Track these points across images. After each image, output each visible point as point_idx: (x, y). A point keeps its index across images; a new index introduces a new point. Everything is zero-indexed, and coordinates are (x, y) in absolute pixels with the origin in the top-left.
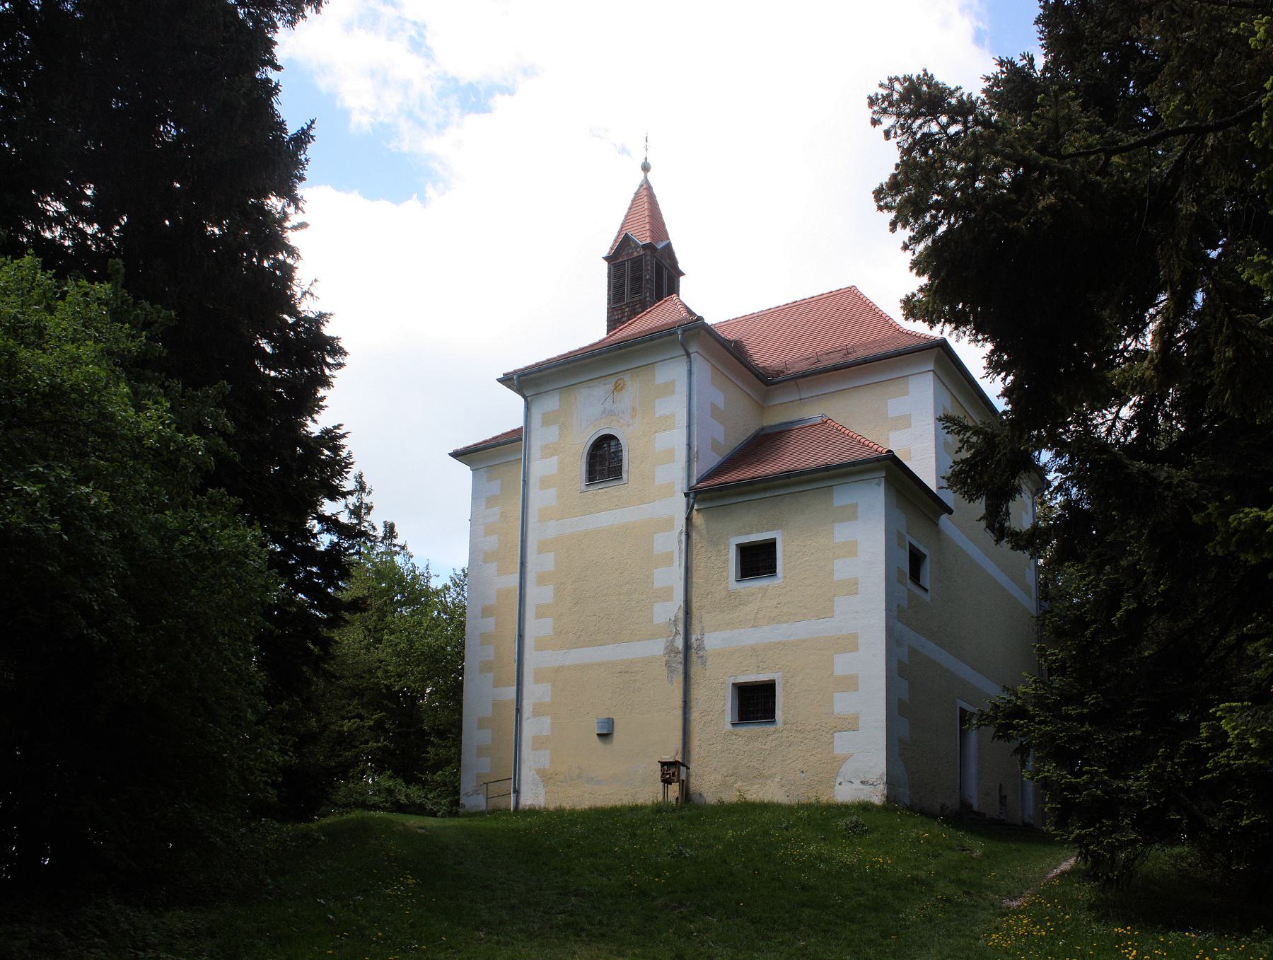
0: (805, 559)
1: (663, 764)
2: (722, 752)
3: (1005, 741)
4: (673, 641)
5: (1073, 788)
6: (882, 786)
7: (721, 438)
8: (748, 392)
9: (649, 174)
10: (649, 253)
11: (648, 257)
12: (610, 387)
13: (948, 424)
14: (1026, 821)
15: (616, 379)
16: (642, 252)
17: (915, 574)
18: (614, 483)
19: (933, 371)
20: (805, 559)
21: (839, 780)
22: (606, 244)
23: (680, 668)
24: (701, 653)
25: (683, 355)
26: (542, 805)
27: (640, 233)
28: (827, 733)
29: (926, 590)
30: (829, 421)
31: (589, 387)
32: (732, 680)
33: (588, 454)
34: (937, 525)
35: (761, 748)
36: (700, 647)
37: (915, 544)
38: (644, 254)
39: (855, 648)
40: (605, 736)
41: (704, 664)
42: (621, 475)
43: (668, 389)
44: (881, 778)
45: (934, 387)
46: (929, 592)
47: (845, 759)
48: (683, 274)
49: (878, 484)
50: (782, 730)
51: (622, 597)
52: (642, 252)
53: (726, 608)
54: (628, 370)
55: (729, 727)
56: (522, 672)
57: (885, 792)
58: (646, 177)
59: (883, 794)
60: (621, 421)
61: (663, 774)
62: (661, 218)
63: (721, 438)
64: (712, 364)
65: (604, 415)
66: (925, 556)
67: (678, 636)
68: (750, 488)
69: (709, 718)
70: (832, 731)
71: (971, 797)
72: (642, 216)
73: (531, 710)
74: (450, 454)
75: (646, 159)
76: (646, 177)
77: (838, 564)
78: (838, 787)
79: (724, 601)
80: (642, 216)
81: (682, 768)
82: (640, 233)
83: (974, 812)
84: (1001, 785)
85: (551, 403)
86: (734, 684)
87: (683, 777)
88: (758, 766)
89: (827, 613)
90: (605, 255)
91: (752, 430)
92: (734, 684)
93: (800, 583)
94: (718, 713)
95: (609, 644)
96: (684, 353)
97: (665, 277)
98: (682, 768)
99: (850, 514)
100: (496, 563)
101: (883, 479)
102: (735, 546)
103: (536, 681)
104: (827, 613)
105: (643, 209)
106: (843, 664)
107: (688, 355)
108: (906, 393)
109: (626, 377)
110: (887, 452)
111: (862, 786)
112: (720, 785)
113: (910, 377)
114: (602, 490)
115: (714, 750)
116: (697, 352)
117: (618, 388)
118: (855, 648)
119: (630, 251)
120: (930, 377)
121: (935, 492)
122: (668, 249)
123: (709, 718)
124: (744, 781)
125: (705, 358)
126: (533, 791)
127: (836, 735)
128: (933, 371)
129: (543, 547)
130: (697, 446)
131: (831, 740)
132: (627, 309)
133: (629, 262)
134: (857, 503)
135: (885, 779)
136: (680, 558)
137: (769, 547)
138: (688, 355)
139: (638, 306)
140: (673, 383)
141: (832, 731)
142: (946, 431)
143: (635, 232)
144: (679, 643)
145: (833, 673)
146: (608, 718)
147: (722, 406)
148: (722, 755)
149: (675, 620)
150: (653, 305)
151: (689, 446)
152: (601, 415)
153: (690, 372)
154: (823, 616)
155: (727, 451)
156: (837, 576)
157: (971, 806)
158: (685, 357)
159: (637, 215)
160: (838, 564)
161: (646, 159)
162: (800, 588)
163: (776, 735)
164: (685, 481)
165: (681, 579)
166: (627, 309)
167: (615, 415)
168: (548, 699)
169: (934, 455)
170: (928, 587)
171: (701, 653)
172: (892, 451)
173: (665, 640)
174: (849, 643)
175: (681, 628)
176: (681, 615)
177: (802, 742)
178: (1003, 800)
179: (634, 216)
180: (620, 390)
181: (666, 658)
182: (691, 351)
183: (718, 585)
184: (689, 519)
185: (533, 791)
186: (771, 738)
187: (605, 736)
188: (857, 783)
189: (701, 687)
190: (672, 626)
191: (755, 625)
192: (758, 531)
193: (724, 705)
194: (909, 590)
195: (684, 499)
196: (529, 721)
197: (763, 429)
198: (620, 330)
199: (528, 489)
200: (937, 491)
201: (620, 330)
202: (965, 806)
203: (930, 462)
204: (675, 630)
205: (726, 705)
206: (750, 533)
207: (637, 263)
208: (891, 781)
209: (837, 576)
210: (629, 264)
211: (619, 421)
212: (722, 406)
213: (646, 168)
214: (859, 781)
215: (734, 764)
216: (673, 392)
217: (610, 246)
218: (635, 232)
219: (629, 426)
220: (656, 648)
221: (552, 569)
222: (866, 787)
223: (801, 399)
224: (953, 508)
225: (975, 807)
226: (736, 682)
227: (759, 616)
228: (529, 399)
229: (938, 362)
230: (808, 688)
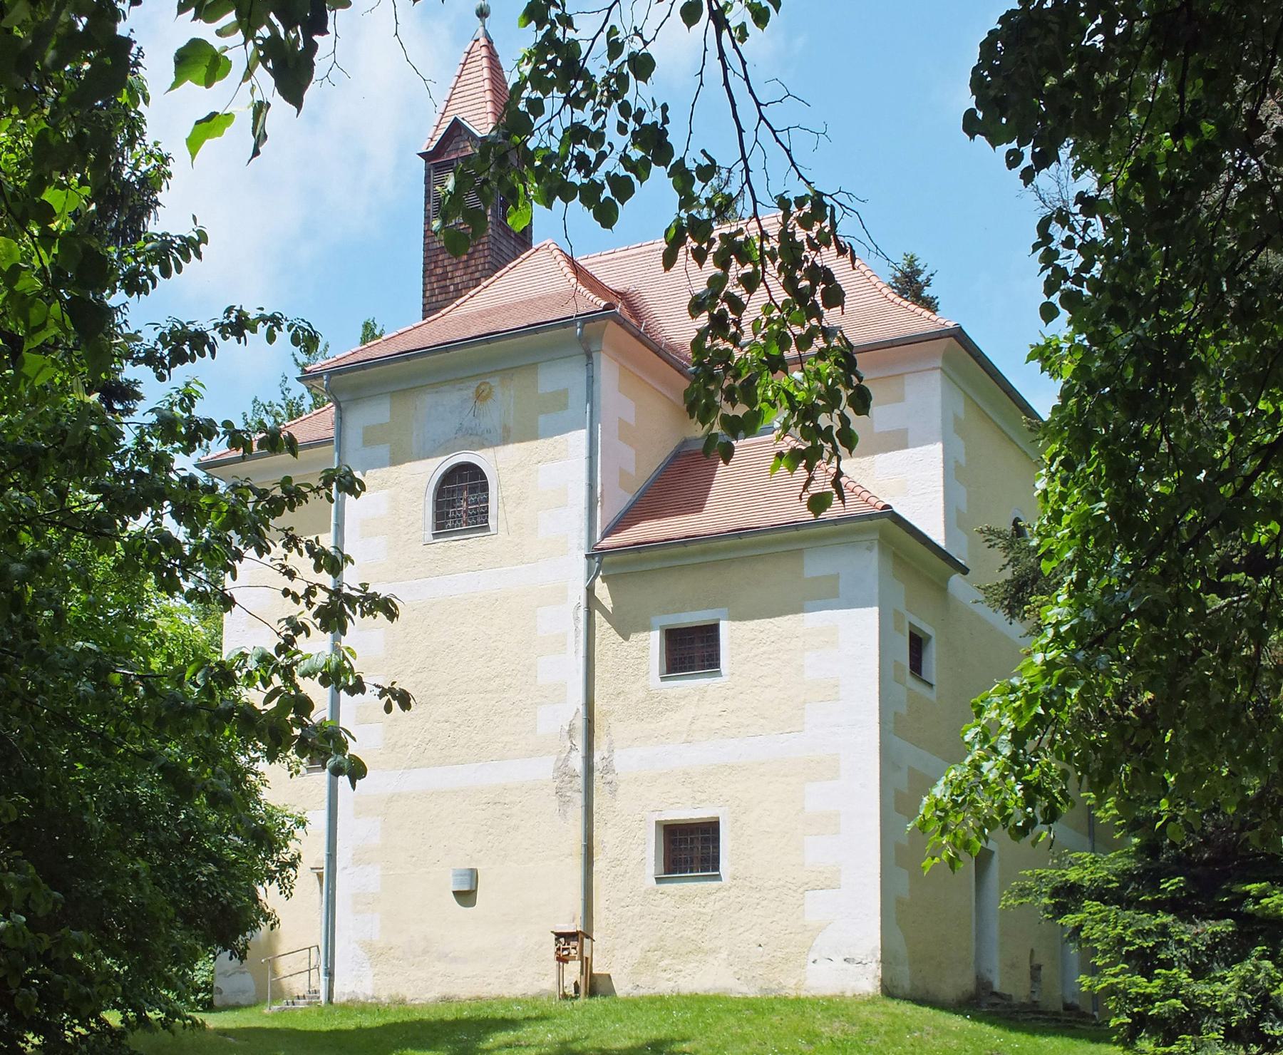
0: (762, 649)
1: (559, 936)
2: (642, 917)
4: (566, 759)
5: (1148, 999)
7: (631, 469)
8: (672, 398)
12: (470, 393)
13: (991, 537)
14: (1069, 1001)
15: (479, 382)
19: (941, 369)
20: (762, 649)
23: (579, 799)
24: (609, 777)
26: (370, 993)
27: (477, 117)
28: (795, 891)
29: (931, 685)
33: (446, 472)
35: (701, 913)
36: (608, 769)
37: (917, 623)
40: (466, 897)
41: (613, 792)
42: (487, 522)
49: (869, 549)
51: (489, 696)
53: (646, 715)
54: (496, 371)
57: (879, 973)
59: (876, 977)
61: (559, 949)
63: (631, 469)
64: (621, 364)
66: (929, 638)
67: (574, 753)
68: (682, 549)
69: (622, 869)
70: (801, 890)
71: (991, 971)
72: (479, 90)
73: (350, 856)
79: (643, 705)
80: (479, 90)
81: (585, 940)
83: (995, 994)
84: (1032, 951)
86: (657, 822)
87: (586, 954)
88: (694, 937)
90: (424, 150)
92: (657, 822)
93: (755, 683)
94: (635, 862)
98: (585, 940)
101: (876, 542)
105: (480, 79)
109: (494, 382)
110: (883, 508)
111: (846, 965)
112: (639, 963)
113: (906, 376)
115: (630, 914)
120: (937, 375)
123: (622, 869)
124: (674, 958)
126: (354, 973)
130: (602, 485)
131: (801, 902)
135: (879, 956)
136: (576, 642)
137: (709, 634)
140: (565, 393)
141: (801, 890)
142: (988, 544)
143: (470, 113)
144: (577, 763)
147: (631, 420)
148: (643, 921)
149: (570, 730)
150: (518, 257)
153: (591, 381)
154: (788, 730)
155: (638, 483)
157: (990, 984)
158: (584, 357)
159: (471, 87)
162: (754, 689)
163: (721, 894)
164: (584, 534)
165: (578, 672)
169: (942, 489)
171: (609, 777)
173: (555, 758)
175: (580, 742)
176: (580, 723)
177: (758, 904)
178: (1036, 970)
179: (466, 88)
180: (485, 399)
181: (556, 784)
183: (633, 682)
184: (590, 590)
185: (354, 973)
186: (713, 897)
187: (466, 897)
188: (838, 960)
189: (609, 825)
190: (567, 736)
191: (690, 739)
192: (693, 609)
194: (909, 689)
195: (583, 562)
196: (347, 871)
198: (472, 297)
201: (472, 297)
202: (983, 986)
203: (935, 498)
204: (569, 744)
205: (648, 851)
208: (887, 960)
212: (631, 420)
214: (842, 958)
215: (660, 934)
216: (565, 406)
218: (470, 113)
220: (543, 770)
222: (851, 967)
225: (997, 987)
226: (663, 818)
227: (694, 727)
229: (951, 371)
230: (768, 829)
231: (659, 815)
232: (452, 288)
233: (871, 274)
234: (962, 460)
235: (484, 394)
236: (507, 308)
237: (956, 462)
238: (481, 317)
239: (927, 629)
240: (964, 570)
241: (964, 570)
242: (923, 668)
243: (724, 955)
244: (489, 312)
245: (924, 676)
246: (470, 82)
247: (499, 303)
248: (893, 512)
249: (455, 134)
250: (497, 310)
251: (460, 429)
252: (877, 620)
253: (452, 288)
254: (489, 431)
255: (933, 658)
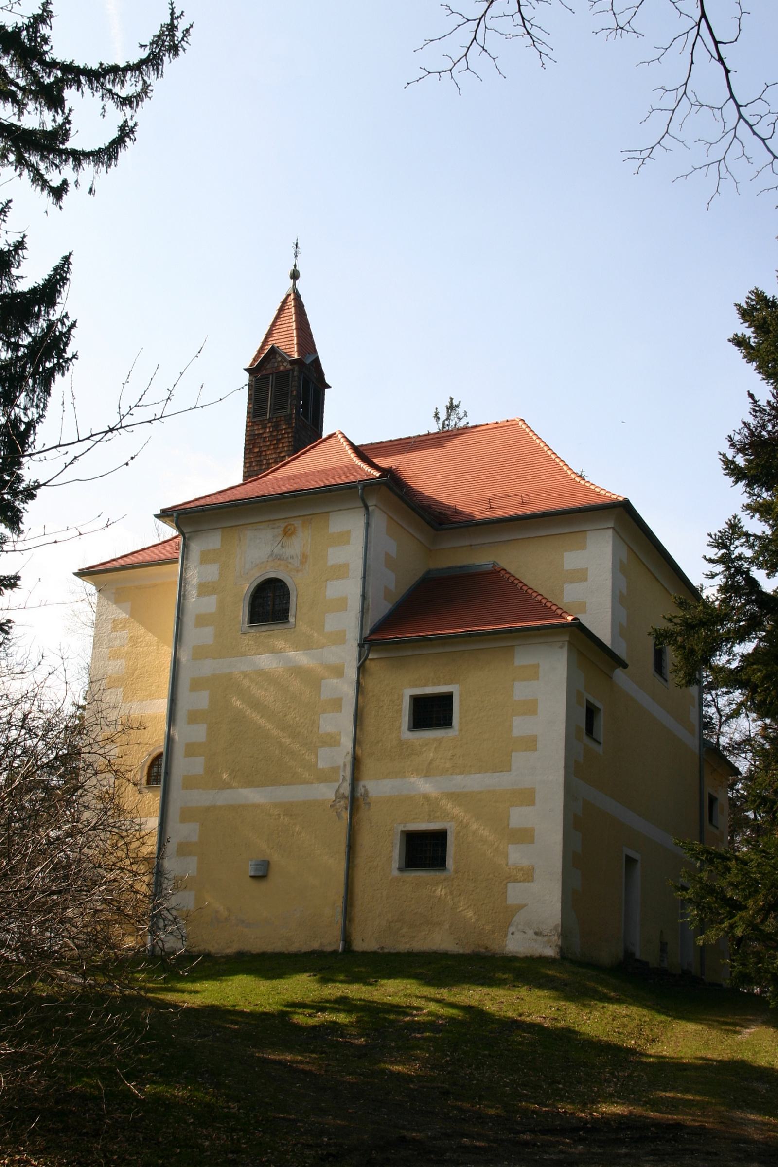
3: (8, 211)
6: (556, 938)
9: (297, 281)
10: (296, 368)
11: (295, 374)
12: (280, 531)
15: (286, 524)
16: (289, 367)
17: (590, 729)
18: (280, 626)
19: (613, 528)
21: (511, 929)
22: (248, 355)
25: (362, 507)
27: (288, 347)
29: (600, 743)
30: (503, 572)
31: (255, 530)
32: (402, 827)
33: (251, 595)
34: (611, 678)
37: (592, 700)
38: (292, 370)
39: (532, 803)
43: (344, 538)
44: (555, 928)
45: (613, 545)
46: (602, 745)
47: (520, 907)
48: (329, 387)
49: (561, 647)
50: (453, 879)
52: (289, 367)
54: (299, 516)
55: (396, 873)
56: (167, 811)
58: (294, 285)
60: (289, 565)
62: (309, 328)
64: (389, 516)
65: (271, 559)
66: (599, 710)
70: (505, 882)
74: (75, 574)
75: (295, 266)
76: (294, 285)
77: (517, 721)
78: (510, 936)
82: (288, 347)
84: (662, 932)
85: (212, 541)
86: (402, 831)
89: (504, 766)
91: (419, 575)
95: (268, 786)
96: (362, 505)
97: (311, 386)
99: (533, 674)
100: (121, 689)
101: (566, 643)
102: (409, 697)
103: (183, 820)
104: (504, 766)
106: (519, 816)
107: (366, 507)
108: (583, 547)
109: (297, 523)
114: (265, 633)
116: (376, 505)
117: (288, 533)
118: (532, 803)
119: (276, 364)
120: (610, 532)
121: (610, 647)
122: (317, 362)
125: (383, 511)
127: (510, 885)
128: (613, 528)
129: (197, 685)
132: (270, 425)
133: (274, 375)
134: (539, 664)
137: (447, 699)
138: (366, 507)
139: (282, 422)
140: (348, 533)
145: (508, 825)
146: (263, 861)
151: (364, 596)
152: (268, 558)
153: (368, 525)
156: (516, 733)
157: (633, 954)
158: (363, 509)
160: (517, 721)
161: (295, 266)
166: (270, 425)
167: (283, 559)
168: (195, 838)
169: (610, 610)
170: (602, 741)
172: (579, 620)
174: (527, 797)
177: (473, 891)
182: (369, 504)
188: (531, 933)
192: (434, 684)
193: (391, 852)
197: (429, 572)
199: (182, 626)
200: (612, 644)
205: (395, 852)
206: (425, 685)
207: (283, 378)
208: (565, 932)
209: (516, 733)
210: (274, 378)
211: (288, 567)
213: (295, 275)
216: (348, 543)
217: (253, 357)
219: (297, 571)
220: (326, 792)
221: (206, 708)
223: (471, 545)
224: (627, 662)
225: (638, 955)
228: (187, 535)
231: (404, 827)
232: (265, 462)
233: (542, 597)
234: (625, 591)
235: (290, 532)
236: (308, 474)
237: (620, 592)
238: (289, 480)
239: (598, 704)
240: (625, 666)
241: (625, 666)
242: (594, 731)
243: (447, 926)
244: (295, 477)
245: (594, 736)
246: (281, 330)
247: (302, 471)
248: (580, 623)
249: (271, 357)
250: (301, 476)
251: (272, 555)
252: (565, 697)
253: (265, 462)
254: (292, 557)
255: (602, 723)
